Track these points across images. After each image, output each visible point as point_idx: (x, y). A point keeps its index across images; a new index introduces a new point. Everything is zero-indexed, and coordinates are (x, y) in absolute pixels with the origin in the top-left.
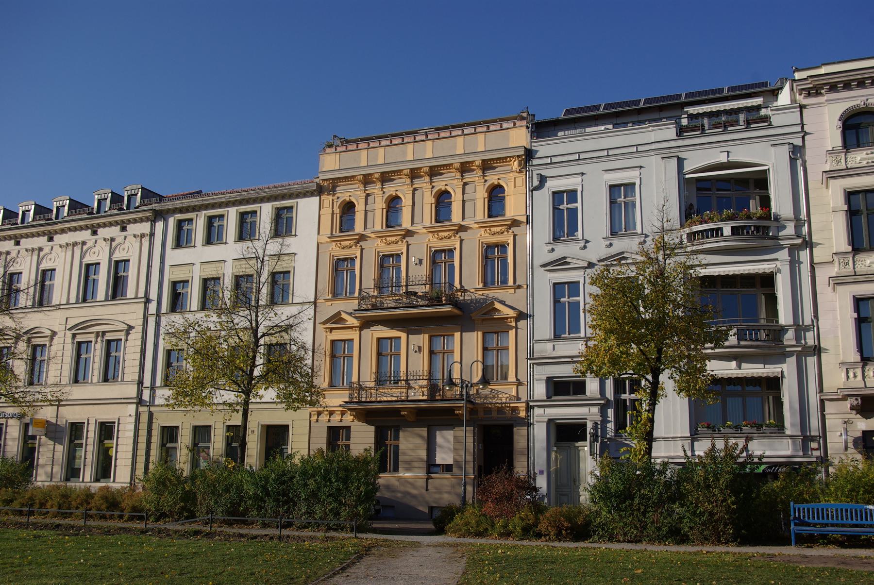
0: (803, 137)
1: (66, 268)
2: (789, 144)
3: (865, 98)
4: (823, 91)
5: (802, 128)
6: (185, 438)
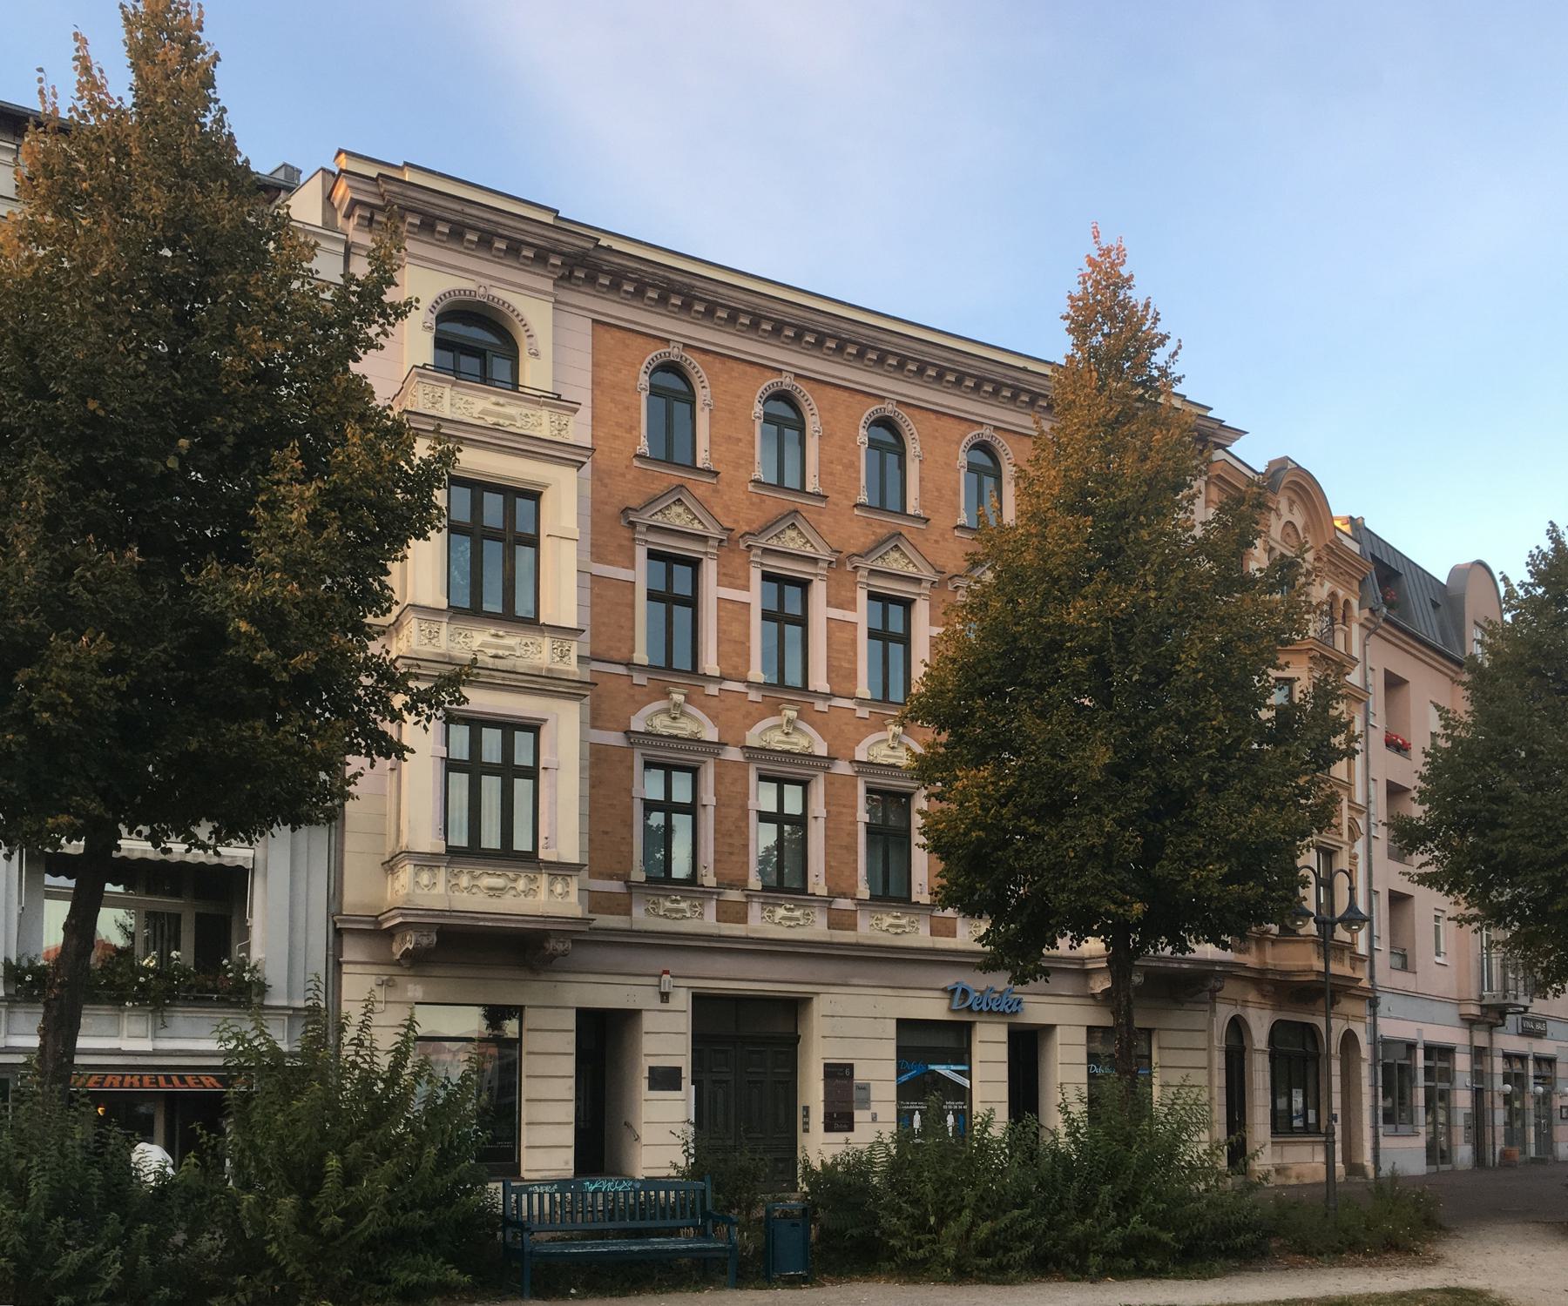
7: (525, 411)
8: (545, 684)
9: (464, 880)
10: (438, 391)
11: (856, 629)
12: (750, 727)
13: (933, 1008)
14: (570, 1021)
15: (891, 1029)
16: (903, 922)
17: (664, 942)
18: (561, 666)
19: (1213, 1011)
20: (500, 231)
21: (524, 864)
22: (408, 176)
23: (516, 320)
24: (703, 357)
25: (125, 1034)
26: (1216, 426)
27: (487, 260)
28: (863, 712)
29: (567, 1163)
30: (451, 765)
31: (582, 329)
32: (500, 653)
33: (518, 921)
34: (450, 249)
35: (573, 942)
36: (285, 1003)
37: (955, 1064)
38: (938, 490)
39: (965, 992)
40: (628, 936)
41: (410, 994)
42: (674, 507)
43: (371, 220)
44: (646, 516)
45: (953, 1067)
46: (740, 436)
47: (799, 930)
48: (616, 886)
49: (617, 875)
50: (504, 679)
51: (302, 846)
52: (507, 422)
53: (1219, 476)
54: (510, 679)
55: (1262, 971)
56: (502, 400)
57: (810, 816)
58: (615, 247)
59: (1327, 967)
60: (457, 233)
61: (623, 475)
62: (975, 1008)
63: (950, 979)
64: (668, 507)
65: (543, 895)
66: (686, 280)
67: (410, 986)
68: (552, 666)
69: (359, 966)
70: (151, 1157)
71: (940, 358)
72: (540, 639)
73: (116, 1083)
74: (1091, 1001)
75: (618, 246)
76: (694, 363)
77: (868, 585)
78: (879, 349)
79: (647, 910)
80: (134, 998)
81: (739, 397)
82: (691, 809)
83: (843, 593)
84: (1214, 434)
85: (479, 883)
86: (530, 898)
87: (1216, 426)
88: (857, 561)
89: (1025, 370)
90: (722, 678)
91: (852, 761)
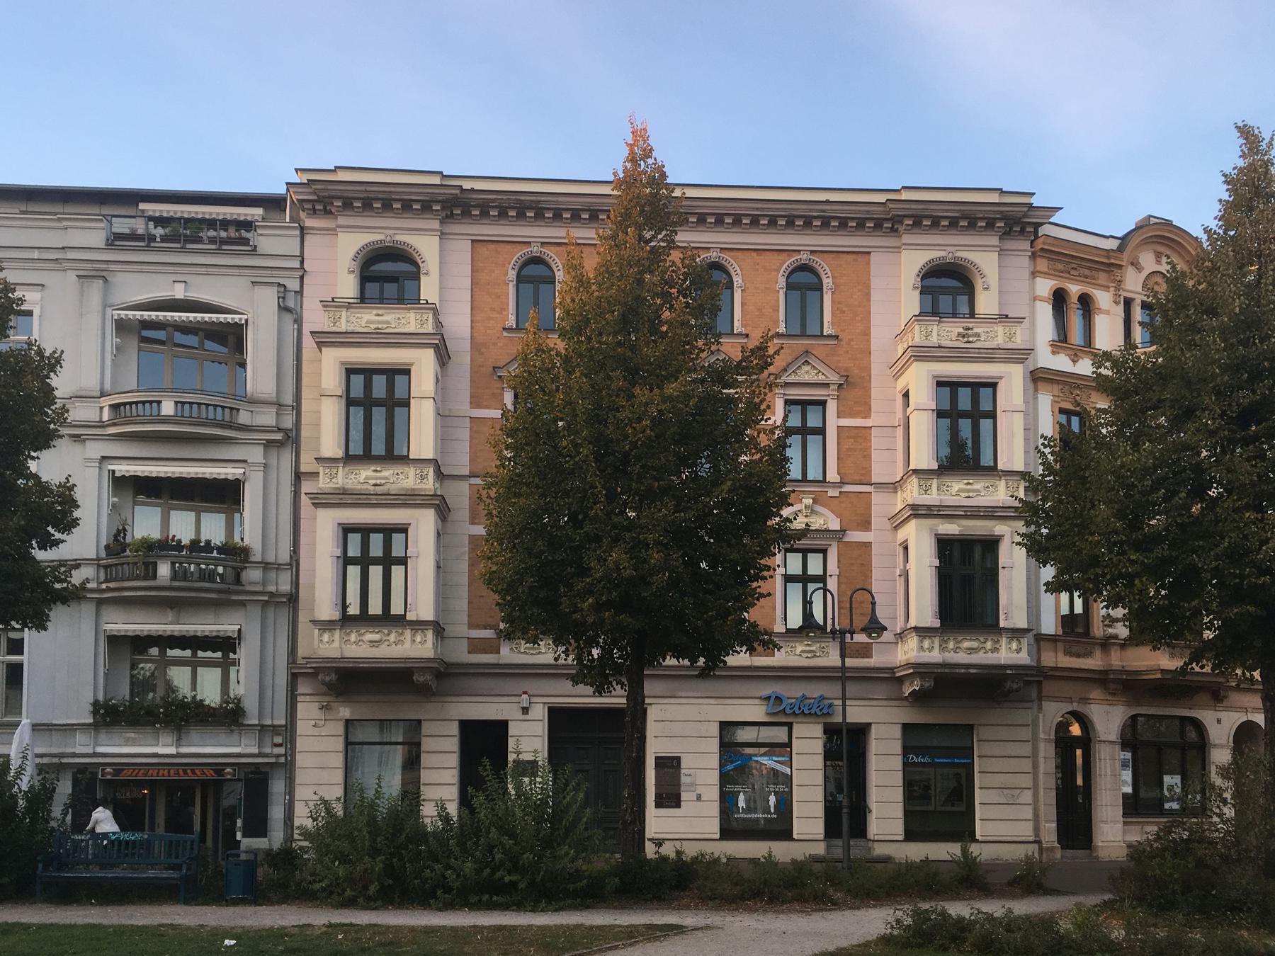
0: (302, 278)
1: (352, 432)
2: (279, 285)
3: (391, 232)
4: (901, 229)
5: (302, 262)
6: (173, 856)
7: (398, 316)
8: (409, 499)
9: (353, 637)
10: (338, 314)
14: (454, 729)
15: (714, 730)
17: (559, 671)
18: (421, 486)
19: (1040, 708)
20: (393, 197)
21: (395, 624)
24: (558, 249)
25: (160, 744)
26: (458, 192)
27: (490, 224)
30: (346, 561)
31: (462, 251)
32: (378, 482)
33: (396, 663)
36: (257, 722)
37: (778, 756)
38: (759, 310)
39: (779, 699)
41: (341, 714)
42: (803, 367)
43: (314, 210)
45: (774, 758)
48: (489, 634)
49: (489, 625)
50: (377, 499)
51: (270, 621)
52: (385, 326)
53: (1042, 249)
54: (382, 499)
55: (1105, 672)
56: (380, 312)
57: (828, 574)
60: (367, 205)
61: (495, 344)
62: (788, 711)
63: (768, 689)
65: (408, 644)
66: (534, 198)
67: (342, 709)
68: (416, 487)
69: (308, 697)
70: (104, 821)
71: (947, 211)
72: (407, 469)
73: (155, 774)
74: (906, 703)
75: (690, 193)
77: (785, 394)
79: (511, 649)
84: (1025, 216)
85: (960, 645)
86: (399, 646)
87: (458, 192)
89: (828, 202)
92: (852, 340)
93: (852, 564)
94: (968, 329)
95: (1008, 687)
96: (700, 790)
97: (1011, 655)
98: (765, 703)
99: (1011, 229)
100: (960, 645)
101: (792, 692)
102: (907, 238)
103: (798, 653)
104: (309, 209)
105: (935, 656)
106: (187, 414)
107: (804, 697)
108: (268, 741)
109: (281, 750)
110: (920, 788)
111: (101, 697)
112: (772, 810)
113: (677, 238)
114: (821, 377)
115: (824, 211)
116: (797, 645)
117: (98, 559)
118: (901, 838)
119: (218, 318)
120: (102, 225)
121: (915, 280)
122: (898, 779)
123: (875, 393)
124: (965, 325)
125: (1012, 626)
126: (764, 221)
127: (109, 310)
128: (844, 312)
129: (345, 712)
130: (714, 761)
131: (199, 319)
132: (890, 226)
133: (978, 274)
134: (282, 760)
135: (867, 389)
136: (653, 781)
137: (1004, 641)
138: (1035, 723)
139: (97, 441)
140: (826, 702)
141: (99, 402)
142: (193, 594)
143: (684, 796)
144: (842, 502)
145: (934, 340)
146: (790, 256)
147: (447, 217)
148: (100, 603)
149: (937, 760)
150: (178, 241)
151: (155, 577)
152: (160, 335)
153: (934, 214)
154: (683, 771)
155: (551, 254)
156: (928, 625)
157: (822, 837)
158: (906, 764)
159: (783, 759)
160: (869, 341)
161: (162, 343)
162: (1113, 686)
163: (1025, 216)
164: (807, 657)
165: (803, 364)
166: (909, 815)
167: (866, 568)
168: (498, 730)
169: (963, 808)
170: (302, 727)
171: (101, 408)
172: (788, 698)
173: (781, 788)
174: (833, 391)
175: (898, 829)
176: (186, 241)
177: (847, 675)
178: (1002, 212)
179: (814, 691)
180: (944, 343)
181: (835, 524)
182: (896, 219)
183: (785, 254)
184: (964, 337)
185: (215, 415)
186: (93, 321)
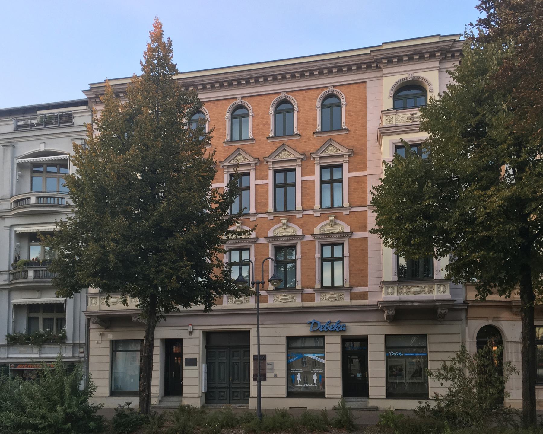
2: (82, 139)
11: (268, 186)
12: (269, 229)
13: (304, 331)
15: (284, 341)
16: (287, 297)
19: (467, 323)
22: (385, 47)
23: (424, 82)
28: (271, 218)
29: (157, 391)
34: (433, 61)
35: (449, 309)
39: (316, 323)
40: (265, 310)
44: (319, 154)
45: (316, 355)
46: (221, 127)
47: (337, 302)
58: (340, 56)
59: (258, 306)
63: (311, 318)
64: (281, 152)
67: (109, 335)
71: (405, 52)
73: (31, 367)
76: (246, 102)
78: (271, 75)
80: (19, 343)
81: (220, 113)
82: (341, 259)
83: (262, 173)
85: (410, 290)
88: (267, 160)
89: (339, 58)
90: (257, 213)
91: (313, 235)
92: (356, 130)
93: (357, 250)
94: (413, 114)
95: (439, 312)
96: (276, 372)
97: (439, 294)
98: (309, 325)
99: (446, 57)
100: (410, 290)
101: (323, 319)
102: (386, 71)
103: (327, 299)
104: (94, 102)
105: (395, 297)
106: (49, 202)
107: (330, 323)
108: (77, 351)
109: (83, 355)
110: (396, 370)
111: (11, 333)
112: (315, 382)
113: (199, 97)
114: (339, 152)
115: (337, 63)
116: (327, 294)
117: (9, 271)
118: (385, 397)
119: (60, 157)
120: (12, 122)
121: (390, 93)
122: (383, 365)
123: (369, 157)
124: (411, 112)
125: (440, 278)
126: (307, 74)
127: (15, 160)
128: (352, 116)
129: (110, 336)
130: (284, 357)
131: (50, 159)
132: (375, 65)
133: (427, 84)
134: (83, 359)
135: (365, 156)
136: (253, 368)
137: (436, 286)
138: (463, 333)
139: (9, 219)
140: (342, 324)
141: (10, 201)
142: (42, 284)
143: (268, 375)
144: (351, 217)
145: (394, 123)
146: (322, 90)
147: (443, 59)
148: (10, 290)
149: (406, 354)
150: (42, 125)
151: (27, 278)
152: (41, 169)
153: (398, 55)
154: (267, 362)
155: (341, 92)
156: (390, 280)
157: (340, 396)
158: (387, 357)
159: (321, 355)
160: (366, 129)
161: (41, 172)
162: (515, 310)
163: (452, 47)
164: (332, 301)
165: (238, 155)
166: (389, 385)
167: (364, 252)
168: (179, 342)
169: (422, 381)
170: (92, 344)
171: (11, 203)
172: (321, 323)
173: (320, 370)
174: (299, 162)
175: (383, 392)
176: (46, 125)
177: (260, 312)
178: (437, 47)
179: (335, 318)
180: (400, 124)
181: (347, 229)
182: (378, 61)
183: (320, 90)
184: (411, 119)
185: (54, 201)
186: (8, 165)
